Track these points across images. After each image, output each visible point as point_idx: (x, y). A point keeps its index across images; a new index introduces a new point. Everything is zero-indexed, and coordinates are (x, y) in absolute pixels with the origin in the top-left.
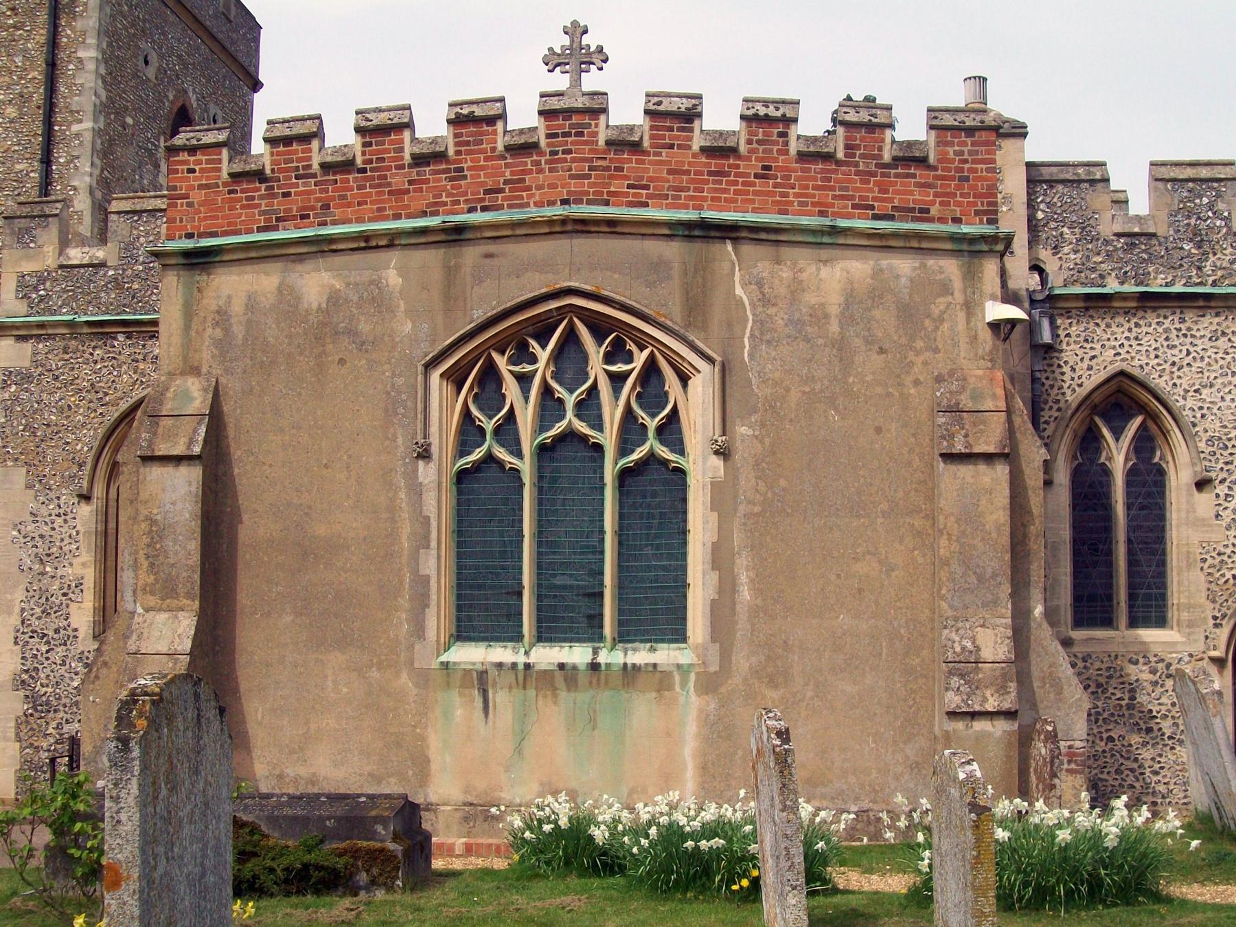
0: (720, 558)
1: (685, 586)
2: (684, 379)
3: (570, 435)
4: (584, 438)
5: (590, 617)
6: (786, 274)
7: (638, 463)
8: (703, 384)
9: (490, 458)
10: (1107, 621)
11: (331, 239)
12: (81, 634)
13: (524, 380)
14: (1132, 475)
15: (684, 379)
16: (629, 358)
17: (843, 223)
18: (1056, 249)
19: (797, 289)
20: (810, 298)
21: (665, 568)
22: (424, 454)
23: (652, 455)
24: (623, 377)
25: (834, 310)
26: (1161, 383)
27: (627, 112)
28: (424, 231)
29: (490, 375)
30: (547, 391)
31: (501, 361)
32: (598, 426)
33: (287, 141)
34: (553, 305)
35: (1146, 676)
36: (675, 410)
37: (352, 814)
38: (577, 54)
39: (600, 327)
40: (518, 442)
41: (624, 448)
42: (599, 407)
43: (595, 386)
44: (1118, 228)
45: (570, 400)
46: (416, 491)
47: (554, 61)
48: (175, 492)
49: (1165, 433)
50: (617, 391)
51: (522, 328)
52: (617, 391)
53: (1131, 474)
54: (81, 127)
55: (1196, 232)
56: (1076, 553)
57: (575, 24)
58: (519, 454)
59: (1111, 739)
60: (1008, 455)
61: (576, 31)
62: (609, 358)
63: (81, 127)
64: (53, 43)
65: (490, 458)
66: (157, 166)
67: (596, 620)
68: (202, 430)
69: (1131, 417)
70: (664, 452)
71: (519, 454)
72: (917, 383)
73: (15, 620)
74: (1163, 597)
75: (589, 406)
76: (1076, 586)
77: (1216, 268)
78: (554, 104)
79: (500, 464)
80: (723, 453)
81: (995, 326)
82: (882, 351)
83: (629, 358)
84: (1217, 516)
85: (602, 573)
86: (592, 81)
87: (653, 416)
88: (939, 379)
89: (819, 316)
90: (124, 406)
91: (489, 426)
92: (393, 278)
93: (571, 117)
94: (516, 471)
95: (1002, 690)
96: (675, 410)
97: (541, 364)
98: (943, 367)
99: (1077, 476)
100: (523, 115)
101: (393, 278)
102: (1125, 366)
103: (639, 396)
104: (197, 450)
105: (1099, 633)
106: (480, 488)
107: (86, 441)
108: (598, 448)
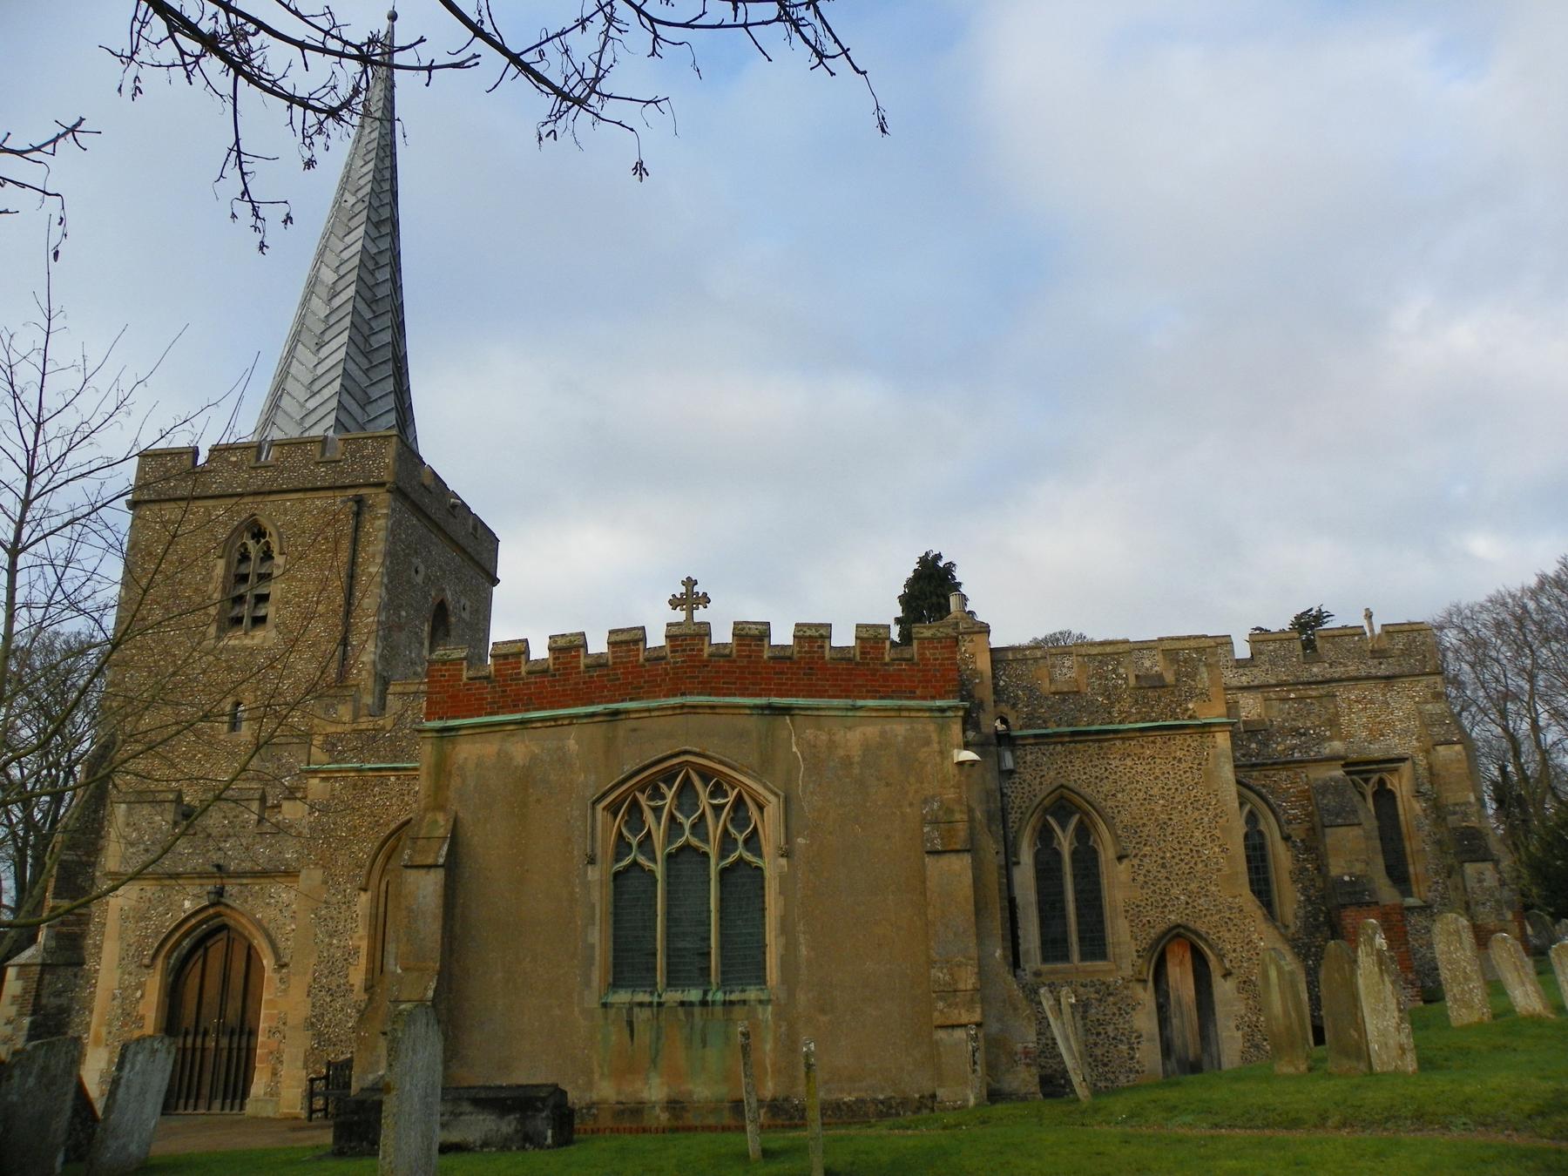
0: (785, 928)
1: (765, 946)
2: (761, 808)
3: (686, 847)
4: (696, 850)
5: (701, 969)
6: (824, 737)
7: (732, 864)
8: (773, 807)
9: (635, 863)
10: (1065, 957)
11: (531, 721)
12: (356, 988)
13: (657, 811)
15: (761, 808)
16: (726, 796)
17: (860, 703)
18: (1014, 706)
19: (832, 745)
20: (841, 752)
21: (750, 934)
22: (592, 861)
23: (741, 858)
24: (721, 807)
26: (1089, 790)
27: (722, 635)
28: (593, 715)
29: (635, 807)
30: (672, 818)
31: (642, 799)
32: (706, 840)
33: (505, 656)
34: (675, 761)
36: (755, 828)
37: (572, 1131)
38: (690, 598)
39: (705, 776)
40: (654, 852)
41: (723, 854)
42: (706, 827)
43: (703, 814)
44: (1053, 689)
45: (687, 824)
46: (586, 885)
47: (675, 603)
48: (426, 888)
49: (1095, 825)
50: (717, 817)
51: (656, 778)
52: (717, 817)
53: (1074, 853)
54: (370, 600)
55: (1106, 688)
56: (1041, 910)
57: (670, 602)
58: (654, 860)
60: (972, 848)
61: (690, 583)
62: (713, 795)
63: (370, 600)
64: (353, 563)
65: (635, 863)
66: (422, 644)
67: (705, 971)
68: (445, 848)
69: (1072, 814)
70: (748, 857)
71: (654, 860)
72: (911, 805)
73: (309, 978)
74: (1103, 938)
75: (699, 827)
76: (1042, 934)
77: (1121, 712)
78: (675, 630)
79: (641, 867)
80: (786, 854)
81: (961, 764)
82: (888, 785)
83: (726, 796)
85: (709, 939)
86: (700, 615)
87: (741, 832)
88: (925, 801)
89: (847, 762)
90: (393, 826)
91: (634, 843)
92: (572, 744)
93: (688, 638)
94: (652, 872)
96: (755, 828)
97: (668, 800)
100: (656, 638)
101: (572, 744)
102: (1063, 781)
103: (732, 820)
104: (441, 861)
105: (1060, 966)
106: (628, 886)
107: (364, 850)
108: (706, 855)
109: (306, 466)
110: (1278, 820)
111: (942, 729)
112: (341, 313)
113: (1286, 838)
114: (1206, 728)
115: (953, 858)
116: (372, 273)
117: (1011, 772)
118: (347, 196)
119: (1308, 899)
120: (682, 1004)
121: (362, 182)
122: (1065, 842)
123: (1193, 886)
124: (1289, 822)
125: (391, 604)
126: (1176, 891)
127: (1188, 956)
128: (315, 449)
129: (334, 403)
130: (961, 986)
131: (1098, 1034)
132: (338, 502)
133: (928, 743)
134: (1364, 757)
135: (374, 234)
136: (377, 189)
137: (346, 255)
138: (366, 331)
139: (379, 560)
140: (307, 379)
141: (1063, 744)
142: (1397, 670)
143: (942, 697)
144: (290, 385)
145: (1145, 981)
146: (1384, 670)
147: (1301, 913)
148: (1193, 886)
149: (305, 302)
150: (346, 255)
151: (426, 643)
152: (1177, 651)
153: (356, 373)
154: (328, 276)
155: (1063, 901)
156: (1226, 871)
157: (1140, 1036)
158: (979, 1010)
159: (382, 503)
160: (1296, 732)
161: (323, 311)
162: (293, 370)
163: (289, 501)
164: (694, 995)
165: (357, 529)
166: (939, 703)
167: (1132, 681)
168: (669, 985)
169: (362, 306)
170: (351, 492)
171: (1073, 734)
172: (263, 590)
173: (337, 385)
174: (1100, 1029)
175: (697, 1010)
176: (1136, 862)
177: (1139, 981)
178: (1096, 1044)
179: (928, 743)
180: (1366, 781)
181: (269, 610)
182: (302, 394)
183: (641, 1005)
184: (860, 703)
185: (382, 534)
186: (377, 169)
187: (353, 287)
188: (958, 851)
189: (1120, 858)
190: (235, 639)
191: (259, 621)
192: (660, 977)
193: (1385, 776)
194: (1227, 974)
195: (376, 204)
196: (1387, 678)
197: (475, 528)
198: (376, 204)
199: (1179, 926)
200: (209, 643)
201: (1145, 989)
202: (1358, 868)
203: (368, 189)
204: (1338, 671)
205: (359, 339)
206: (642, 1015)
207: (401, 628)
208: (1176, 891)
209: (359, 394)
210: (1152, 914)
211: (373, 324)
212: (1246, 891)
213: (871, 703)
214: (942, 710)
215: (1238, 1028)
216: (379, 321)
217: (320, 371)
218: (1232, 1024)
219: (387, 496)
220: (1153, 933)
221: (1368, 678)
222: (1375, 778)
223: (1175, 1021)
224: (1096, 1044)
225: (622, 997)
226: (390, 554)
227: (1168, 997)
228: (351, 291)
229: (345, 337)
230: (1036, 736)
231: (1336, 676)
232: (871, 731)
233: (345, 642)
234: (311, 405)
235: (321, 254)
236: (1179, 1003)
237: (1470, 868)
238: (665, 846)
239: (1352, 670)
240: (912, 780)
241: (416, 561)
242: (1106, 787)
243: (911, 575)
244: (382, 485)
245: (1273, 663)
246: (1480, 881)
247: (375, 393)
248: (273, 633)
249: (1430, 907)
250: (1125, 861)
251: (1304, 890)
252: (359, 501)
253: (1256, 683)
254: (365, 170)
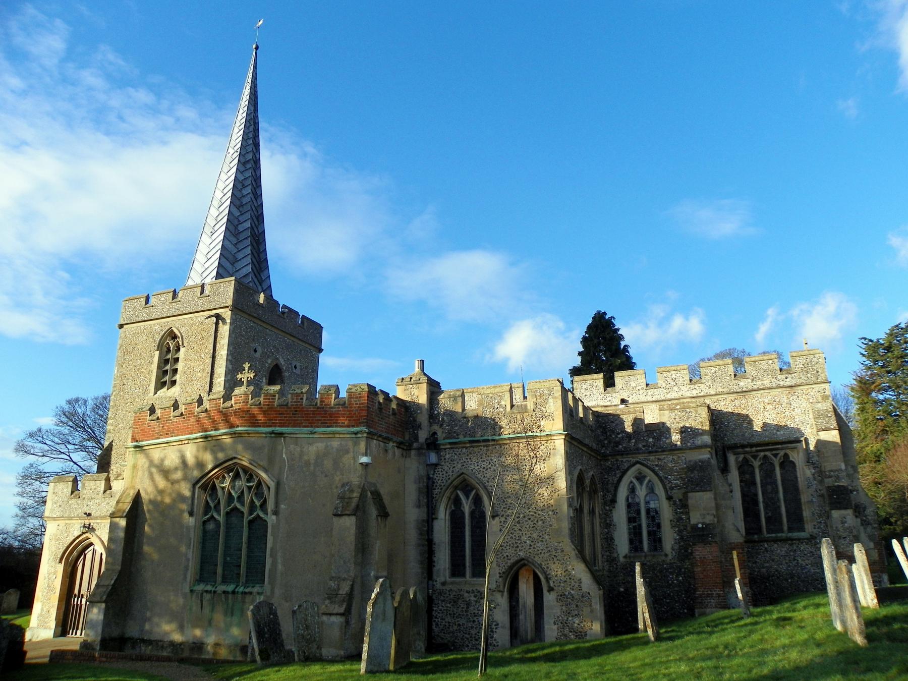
9: (258, 516)
14: (472, 513)
18: (441, 425)
19: (302, 454)
20: (306, 458)
25: (313, 462)
31: (217, 482)
34: (230, 462)
35: (473, 599)
59: (459, 625)
82: (326, 476)
84: (501, 530)
89: (308, 463)
95: (341, 606)
98: (346, 480)
99: (453, 514)
108: (242, 513)
110: (665, 487)
111: (356, 444)
113: (669, 498)
115: (346, 518)
117: (436, 465)
119: (682, 538)
120: (224, 592)
126: (524, 538)
127: (531, 578)
130: (341, 592)
131: (474, 621)
133: (347, 452)
134: (773, 440)
135: (242, 169)
138: (236, 223)
141: (466, 448)
142: (799, 381)
146: (789, 382)
147: (676, 547)
148: (535, 535)
155: (465, 542)
156: (555, 526)
157: (497, 625)
158: (344, 606)
164: (230, 588)
168: (223, 582)
169: (234, 210)
171: (471, 442)
174: (475, 619)
175: (230, 596)
176: (503, 519)
177: (499, 591)
178: (472, 627)
180: (776, 455)
181: (177, 377)
183: (207, 591)
184: (317, 430)
188: (349, 515)
189: (493, 517)
191: (174, 383)
193: (788, 452)
194: (551, 589)
199: (523, 559)
201: (502, 596)
202: (709, 519)
203: (239, 145)
206: (207, 597)
208: (524, 538)
209: (231, 258)
211: (240, 218)
212: (567, 540)
213: (321, 430)
215: (555, 624)
220: (510, 562)
222: (782, 453)
224: (472, 627)
225: (201, 587)
227: (518, 601)
230: (450, 443)
231: (755, 387)
232: (321, 446)
234: (207, 265)
236: (524, 607)
237: (836, 514)
238: (225, 508)
240: (338, 473)
241: (253, 345)
243: (590, 321)
246: (843, 523)
247: (240, 255)
250: (497, 519)
251: (680, 532)
253: (702, 394)
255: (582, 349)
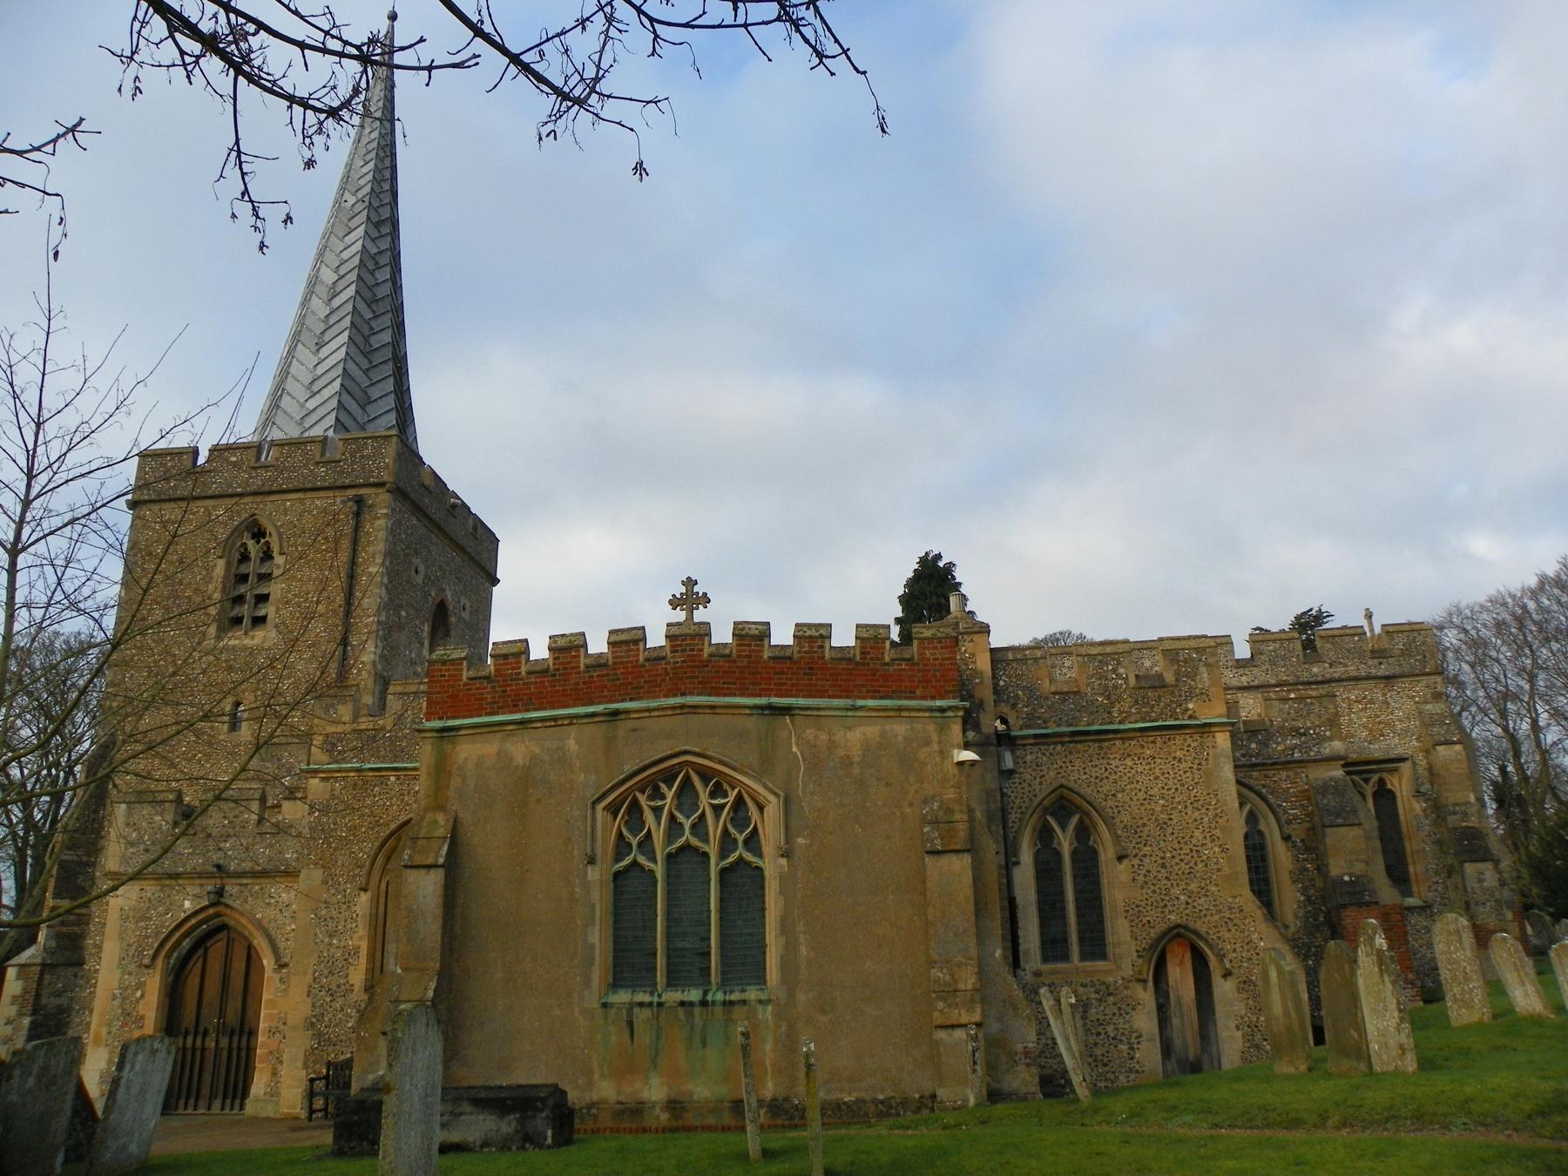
0: (785, 928)
1: (765, 946)
2: (761, 808)
3: (686, 847)
4: (696, 850)
5: (701, 969)
6: (824, 737)
7: (732, 864)
8: (773, 807)
9: (635, 863)
10: (1065, 957)
11: (531, 721)
12: (356, 988)
13: (657, 811)
15: (761, 808)
16: (726, 796)
17: (860, 703)
18: (1014, 706)
19: (832, 745)
20: (841, 752)
21: (750, 934)
22: (592, 861)
23: (741, 858)
24: (721, 807)
26: (1089, 790)
27: (722, 635)
28: (593, 715)
29: (635, 807)
30: (672, 818)
31: (642, 799)
32: (706, 840)
33: (505, 656)
34: (675, 761)
36: (755, 828)
37: (572, 1131)
38: (690, 598)
39: (705, 776)
40: (654, 852)
41: (723, 854)
42: (706, 827)
43: (703, 814)
44: (1053, 689)
45: (687, 824)
46: (586, 885)
47: (675, 603)
48: (426, 888)
49: (1095, 825)
50: (717, 817)
51: (656, 778)
52: (717, 817)
53: (1074, 853)
54: (370, 600)
55: (1106, 688)
56: (1041, 910)
57: (670, 602)
58: (654, 860)
60: (972, 848)
61: (690, 583)
62: (713, 795)
63: (370, 600)
64: (353, 563)
65: (635, 863)
66: (422, 644)
67: (705, 971)
68: (445, 848)
69: (1072, 814)
70: (748, 857)
71: (654, 860)
72: (911, 805)
73: (309, 978)
74: (1103, 938)
75: (699, 827)
76: (1042, 934)
77: (1121, 712)
78: (675, 630)
79: (641, 867)
80: (786, 854)
81: (961, 764)
82: (888, 785)
83: (726, 796)
85: (709, 939)
86: (700, 615)
87: (741, 832)
88: (925, 801)
89: (847, 762)
90: (393, 826)
91: (634, 843)
92: (572, 744)
93: (688, 638)
94: (652, 872)
96: (755, 828)
97: (668, 800)
100: (656, 638)
101: (572, 744)
102: (1063, 781)
103: (732, 820)
104: (441, 861)
105: (1060, 966)
106: (628, 886)
107: (364, 850)
108: (706, 855)
109: (306, 466)
110: (1278, 820)
111: (942, 729)
112: (341, 313)
113: (1286, 838)
114: (1206, 728)
115: (953, 858)
116: (372, 273)
117: (1011, 772)
118: (347, 196)
119: (1308, 899)
120: (682, 1004)
121: (362, 182)
122: (1065, 842)
123: (1193, 886)
124: (1289, 822)
125: (391, 604)
126: (1176, 891)
127: (1188, 956)
128: (315, 449)
129: (334, 403)
130: (961, 986)
131: (1098, 1034)
132: (338, 502)
133: (928, 743)
134: (1364, 757)
135: (374, 234)
136: (377, 189)
137: (346, 255)
138: (366, 331)
139: (379, 560)
140: (307, 379)
141: (1063, 744)
142: (1397, 670)
143: (942, 697)
144: (290, 385)
145: (1145, 981)
146: (1384, 670)
147: (1301, 913)
148: (1193, 886)
149: (305, 302)
150: (346, 255)
151: (426, 643)
152: (1177, 651)
153: (356, 373)
154: (328, 276)
155: (1063, 901)
156: (1226, 871)
157: (1140, 1036)
158: (979, 1010)
159: (382, 503)
160: (1296, 732)
161: (323, 311)
162: (293, 370)
163: (289, 501)
164: (694, 995)
165: (357, 529)
166: (939, 703)
167: (1132, 681)
168: (669, 985)
169: (362, 306)
170: (351, 492)
171: (1073, 734)
172: (263, 590)
173: (337, 385)
174: (1100, 1029)
175: (697, 1010)
176: (1136, 862)
177: (1139, 981)
178: (1096, 1044)
179: (928, 743)
180: (1366, 781)
181: (269, 610)
182: (302, 394)
183: (641, 1005)
184: (860, 703)
185: (382, 534)
186: (377, 169)
187: (353, 287)
188: (958, 851)
189: (1120, 858)
190: (235, 639)
191: (259, 621)
192: (660, 977)
193: (1385, 776)
194: (1227, 974)
195: (376, 204)
196: (1387, 678)
197: (475, 528)
198: (376, 204)
199: (1179, 926)
200: (209, 643)
201: (1145, 989)
202: (1358, 868)
203: (368, 189)
204: (1338, 671)
205: (359, 339)
206: (642, 1015)
207: (401, 628)
208: (1176, 891)
209: (359, 394)
210: (1152, 914)
211: (373, 324)
212: (1246, 891)
213: (871, 703)
214: (942, 710)
215: (1238, 1028)
216: (379, 321)
217: (320, 371)
218: (1232, 1024)
219: (387, 496)
220: (1153, 933)
221: (1368, 678)
222: (1375, 778)
223: (1175, 1021)
224: (1096, 1044)
225: (622, 997)
226: (390, 554)
227: (1168, 997)
228: (351, 291)
229: (345, 337)
230: (1036, 736)
231: (1336, 676)
232: (871, 731)
233: (345, 642)
234: (311, 405)
235: (321, 254)
236: (1179, 1003)
237: (1470, 868)
238: (665, 846)
239: (1352, 670)
240: (912, 780)
241: (416, 561)
242: (1106, 787)
243: (911, 575)
244: (382, 485)
245: (1273, 663)
246: (1480, 881)
247: (375, 393)
248: (273, 633)
249: (1430, 907)
250: (1125, 861)
251: (1304, 890)
252: (359, 501)
253: (1256, 683)
254: (365, 170)
255: (900, 615)
